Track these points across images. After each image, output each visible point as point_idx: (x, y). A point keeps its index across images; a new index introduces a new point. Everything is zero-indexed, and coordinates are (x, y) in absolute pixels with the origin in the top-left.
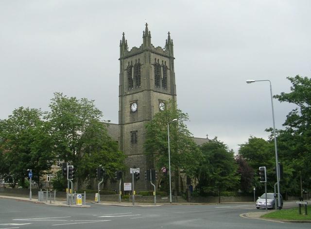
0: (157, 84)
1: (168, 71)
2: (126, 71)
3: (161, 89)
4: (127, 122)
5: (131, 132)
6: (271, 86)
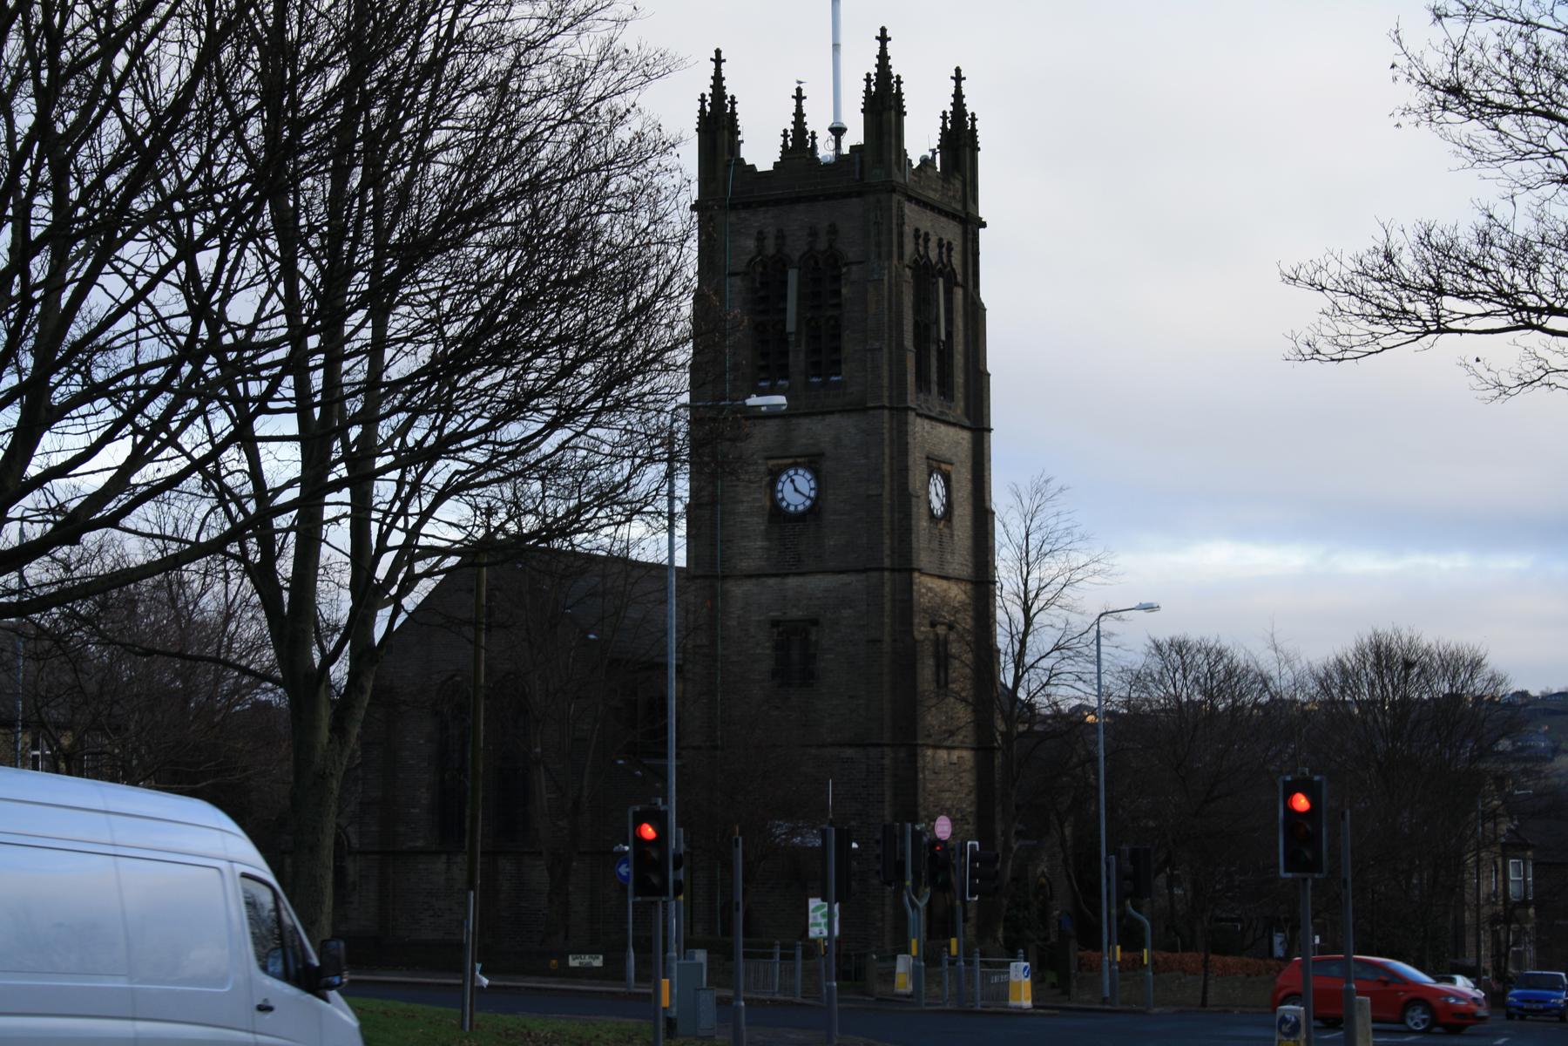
0: (922, 382)
1: (959, 293)
2: (737, 281)
3: (935, 403)
4: (745, 565)
5: (775, 623)
6: (450, 524)
